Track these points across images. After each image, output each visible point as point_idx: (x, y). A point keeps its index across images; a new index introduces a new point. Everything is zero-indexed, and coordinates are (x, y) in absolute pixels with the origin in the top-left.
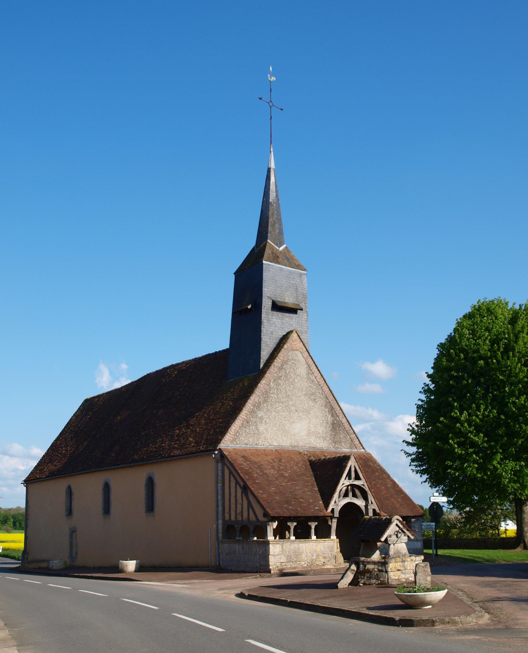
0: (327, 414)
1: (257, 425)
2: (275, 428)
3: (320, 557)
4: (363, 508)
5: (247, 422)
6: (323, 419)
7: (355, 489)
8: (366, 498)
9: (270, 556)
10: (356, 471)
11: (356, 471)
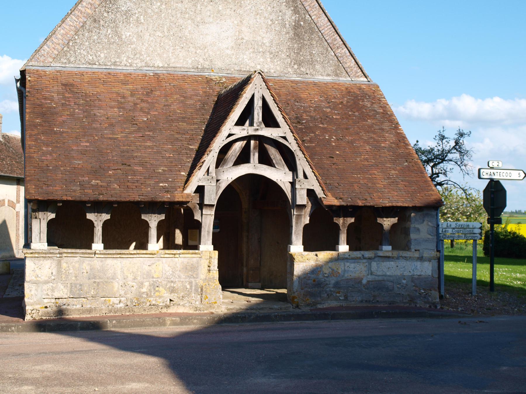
0: (283, 7)
1: (117, 27)
2: (159, 34)
3: (161, 289)
4: (287, 189)
5: (95, 21)
6: (273, 17)
7: (268, 146)
8: (292, 166)
9: (26, 285)
10: (265, 106)
11: (265, 106)
